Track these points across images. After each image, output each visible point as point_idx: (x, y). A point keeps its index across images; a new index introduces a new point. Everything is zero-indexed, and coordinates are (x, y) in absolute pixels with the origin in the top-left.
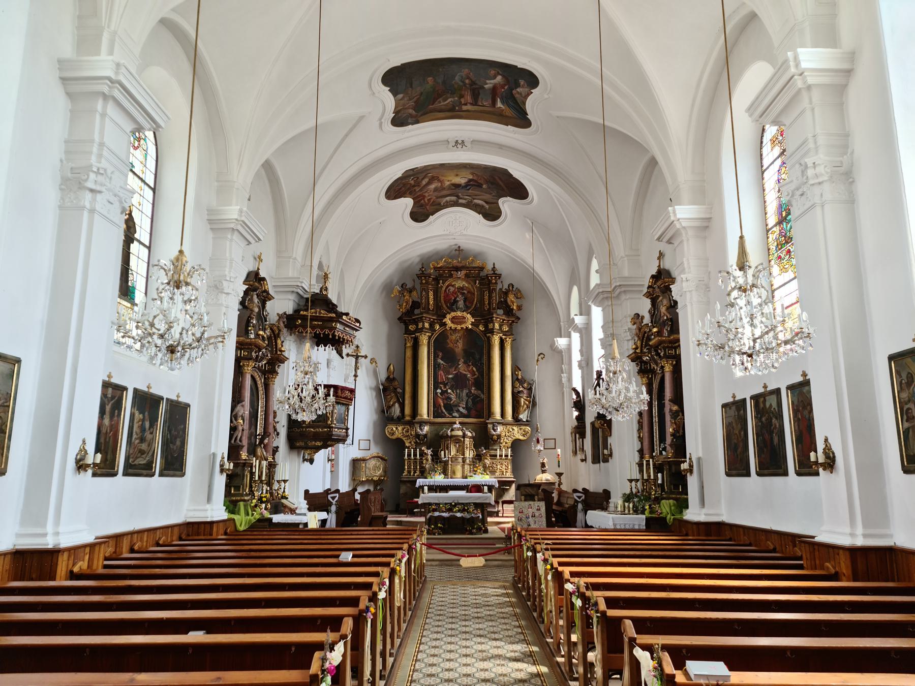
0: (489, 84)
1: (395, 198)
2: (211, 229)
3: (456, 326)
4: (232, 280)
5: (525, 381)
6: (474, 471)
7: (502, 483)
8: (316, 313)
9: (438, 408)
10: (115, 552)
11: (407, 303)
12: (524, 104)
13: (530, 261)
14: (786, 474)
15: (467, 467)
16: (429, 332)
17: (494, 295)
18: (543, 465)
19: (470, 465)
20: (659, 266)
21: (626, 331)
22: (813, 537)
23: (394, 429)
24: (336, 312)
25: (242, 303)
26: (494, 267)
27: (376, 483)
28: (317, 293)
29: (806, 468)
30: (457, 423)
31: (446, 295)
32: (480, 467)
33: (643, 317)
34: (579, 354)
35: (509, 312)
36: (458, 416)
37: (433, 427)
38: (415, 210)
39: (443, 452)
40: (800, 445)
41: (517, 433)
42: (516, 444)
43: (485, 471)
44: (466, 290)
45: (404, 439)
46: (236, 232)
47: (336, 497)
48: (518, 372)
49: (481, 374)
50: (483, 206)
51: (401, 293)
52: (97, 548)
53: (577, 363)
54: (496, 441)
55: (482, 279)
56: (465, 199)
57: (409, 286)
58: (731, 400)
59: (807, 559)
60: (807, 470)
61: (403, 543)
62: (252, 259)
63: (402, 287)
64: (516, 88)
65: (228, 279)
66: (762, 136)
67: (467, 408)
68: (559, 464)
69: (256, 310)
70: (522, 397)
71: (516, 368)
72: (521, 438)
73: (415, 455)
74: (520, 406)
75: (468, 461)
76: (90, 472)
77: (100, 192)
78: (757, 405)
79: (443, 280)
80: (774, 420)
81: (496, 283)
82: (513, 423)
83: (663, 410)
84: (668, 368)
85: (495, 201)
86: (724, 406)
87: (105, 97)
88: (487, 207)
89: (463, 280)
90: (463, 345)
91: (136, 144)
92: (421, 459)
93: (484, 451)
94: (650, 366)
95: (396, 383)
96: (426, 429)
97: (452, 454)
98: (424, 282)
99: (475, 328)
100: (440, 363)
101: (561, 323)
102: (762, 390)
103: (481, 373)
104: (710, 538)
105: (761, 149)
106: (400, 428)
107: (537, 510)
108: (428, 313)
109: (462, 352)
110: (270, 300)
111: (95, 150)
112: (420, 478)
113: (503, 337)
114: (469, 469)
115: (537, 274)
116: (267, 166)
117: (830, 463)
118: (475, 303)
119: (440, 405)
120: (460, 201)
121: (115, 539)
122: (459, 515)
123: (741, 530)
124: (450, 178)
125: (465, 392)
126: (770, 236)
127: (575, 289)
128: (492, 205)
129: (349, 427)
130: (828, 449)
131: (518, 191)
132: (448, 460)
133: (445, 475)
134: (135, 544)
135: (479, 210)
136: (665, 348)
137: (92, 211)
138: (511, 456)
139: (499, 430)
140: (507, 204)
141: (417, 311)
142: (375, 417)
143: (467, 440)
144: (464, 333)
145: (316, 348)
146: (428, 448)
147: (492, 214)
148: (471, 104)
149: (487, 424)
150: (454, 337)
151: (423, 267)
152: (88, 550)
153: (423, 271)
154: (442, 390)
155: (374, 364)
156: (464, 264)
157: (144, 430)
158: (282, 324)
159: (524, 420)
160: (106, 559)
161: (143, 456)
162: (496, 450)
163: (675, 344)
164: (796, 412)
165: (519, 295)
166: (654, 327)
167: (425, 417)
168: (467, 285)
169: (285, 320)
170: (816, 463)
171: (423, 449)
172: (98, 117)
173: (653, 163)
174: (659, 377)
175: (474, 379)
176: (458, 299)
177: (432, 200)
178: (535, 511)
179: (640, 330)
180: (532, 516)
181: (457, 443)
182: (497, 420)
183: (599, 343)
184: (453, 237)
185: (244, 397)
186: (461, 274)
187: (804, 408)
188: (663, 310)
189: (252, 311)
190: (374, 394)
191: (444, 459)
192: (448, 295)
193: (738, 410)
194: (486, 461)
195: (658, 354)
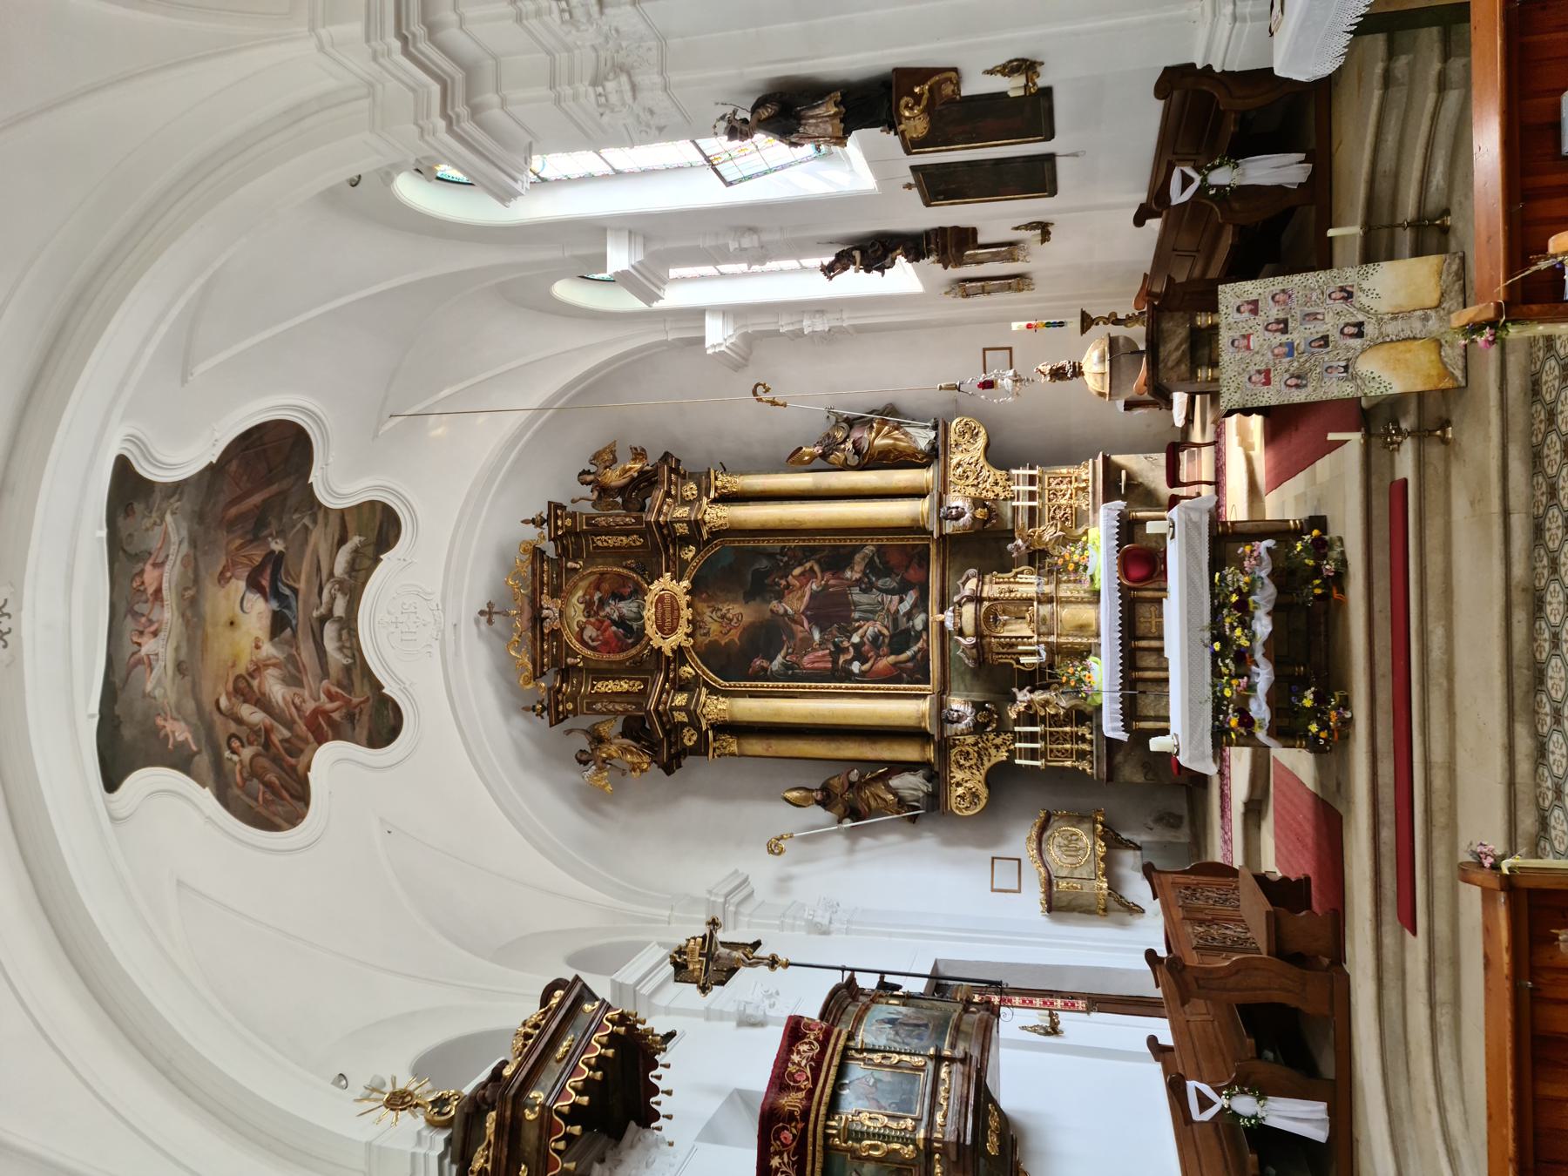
3: (683, 622)
5: (828, 435)
6: (1076, 571)
7: (1110, 493)
9: (903, 670)
11: (625, 750)
13: (512, 422)
15: (1065, 591)
17: (602, 521)
18: (1058, 374)
19: (1058, 582)
23: (960, 791)
26: (533, 521)
27: (1114, 841)
30: (940, 617)
31: (606, 646)
32: (1065, 552)
35: (644, 482)
36: (922, 616)
37: (954, 685)
38: (365, 733)
39: (1024, 660)
41: (968, 453)
42: (999, 457)
43: (1076, 541)
44: (592, 597)
45: (987, 765)
47: (1198, 1091)
48: (805, 454)
49: (809, 552)
50: (356, 551)
54: (990, 510)
55: (564, 553)
56: (333, 599)
57: (583, 743)
63: (585, 763)
67: (901, 591)
68: (1054, 325)
70: (871, 444)
71: (795, 462)
72: (981, 442)
73: (1032, 737)
74: (895, 447)
75: (1048, 589)
79: (567, 656)
81: (573, 516)
82: (941, 463)
85: (334, 522)
88: (355, 541)
89: (566, 602)
90: (734, 601)
93: (1019, 542)
96: (957, 704)
97: (1029, 633)
98: (570, 706)
99: (691, 571)
101: (670, 337)
106: (959, 775)
107: (1255, 311)
109: (752, 603)
112: (1099, 726)
113: (712, 495)
114: (1071, 586)
117: (1025, 67)
119: (895, 665)
120: (339, 609)
122: (1263, 626)
124: (246, 644)
125: (857, 596)
128: (351, 526)
132: (1047, 643)
133: (1089, 652)
135: (367, 563)
137: (795, 918)
138: (1031, 468)
139: (959, 503)
143: (990, 590)
144: (704, 601)
145: (661, 1122)
149: (943, 537)
150: (714, 627)
151: (534, 709)
153: (544, 709)
154: (853, 659)
155: (783, 844)
156: (526, 601)
159: (932, 434)
162: (1015, 509)
165: (605, 457)
167: (924, 706)
168: (580, 593)
171: (1013, 716)
175: (823, 571)
176: (615, 616)
177: (334, 689)
178: (1261, 319)
180: (1285, 331)
181: (996, 619)
182: (931, 509)
184: (450, 628)
186: (550, 607)
190: (866, 842)
191: (1044, 654)
192: (605, 643)
194: (1047, 537)
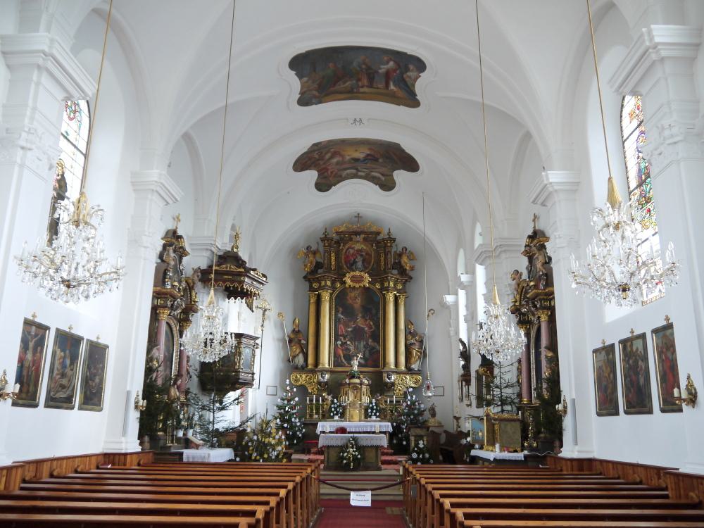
0: (383, 69)
1: (302, 169)
2: (134, 190)
3: (355, 284)
4: (151, 235)
8: (227, 268)
10: (35, 476)
11: (311, 263)
12: (414, 86)
13: (421, 226)
14: (650, 412)
17: (389, 256)
20: (534, 227)
21: (508, 284)
22: (678, 469)
24: (245, 268)
25: (161, 257)
28: (229, 251)
29: (671, 405)
33: (521, 274)
34: (465, 308)
35: (403, 272)
40: (664, 385)
45: (307, 386)
46: (156, 194)
50: (379, 178)
51: (306, 255)
52: (14, 471)
53: (463, 318)
55: (378, 242)
56: (364, 172)
57: (314, 248)
58: (602, 345)
59: (672, 489)
60: (671, 407)
61: (295, 476)
62: (172, 220)
63: (307, 249)
64: (406, 72)
65: (147, 233)
66: (622, 111)
69: (172, 263)
71: (408, 322)
76: (10, 401)
77: (30, 149)
78: (624, 349)
80: (640, 363)
81: (391, 246)
83: (540, 357)
84: (544, 318)
86: (595, 351)
87: (39, 67)
88: (383, 178)
90: (362, 301)
91: (72, 115)
94: (528, 317)
97: (350, 400)
98: (327, 244)
99: (372, 287)
102: (629, 335)
103: (377, 326)
104: (582, 473)
105: (621, 122)
106: (304, 376)
108: (329, 272)
110: (186, 255)
111: (28, 113)
115: (428, 238)
116: (187, 137)
117: (693, 399)
120: (360, 173)
121: (35, 465)
123: (611, 465)
124: (349, 153)
125: (363, 343)
126: (632, 197)
127: (461, 252)
129: (255, 371)
130: (691, 386)
131: (410, 164)
134: (54, 470)
136: (541, 300)
139: (393, 378)
140: (400, 176)
141: (320, 271)
142: (281, 365)
143: (364, 387)
146: (328, 395)
147: (387, 185)
148: (367, 86)
149: (382, 373)
152: (5, 472)
157: (66, 367)
158: (196, 278)
160: (24, 481)
161: (64, 390)
163: (550, 296)
164: (660, 353)
165: (412, 257)
166: (531, 281)
167: (327, 366)
169: (199, 274)
170: (680, 398)
172: (33, 86)
173: (528, 136)
174: (536, 327)
177: (334, 173)
179: (518, 285)
183: (483, 297)
185: (160, 342)
187: (668, 349)
188: (539, 265)
189: (168, 264)
190: (281, 344)
193: (608, 354)
195: (535, 306)
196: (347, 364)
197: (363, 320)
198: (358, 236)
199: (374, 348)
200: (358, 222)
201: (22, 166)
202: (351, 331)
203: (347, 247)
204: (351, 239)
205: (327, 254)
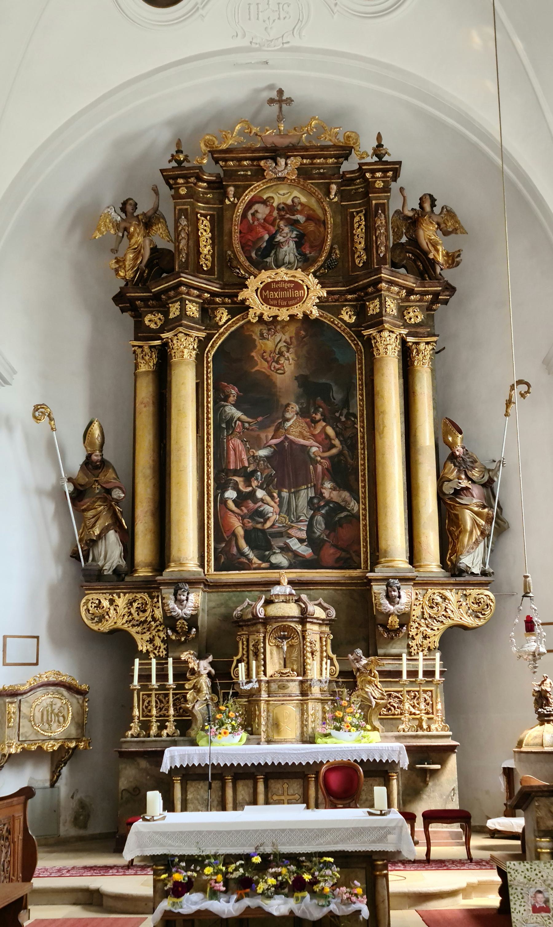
3: (274, 311)
5: (474, 461)
6: (335, 719)
9: (228, 543)
11: (138, 252)
15: (314, 708)
16: (199, 330)
17: (381, 221)
26: (380, 146)
30: (285, 581)
39: (242, 667)
43: (366, 719)
44: (300, 212)
45: (133, 631)
63: (123, 209)
72: (469, 621)
73: (162, 676)
74: (462, 531)
75: (316, 691)
79: (236, 187)
81: (386, 189)
82: (446, 580)
89: (293, 184)
90: (298, 366)
92: (180, 687)
93: (364, 661)
95: (111, 475)
97: (270, 672)
98: (183, 191)
99: (328, 319)
100: (232, 418)
109: (296, 383)
112: (175, 743)
114: (320, 714)
118: (327, 247)
119: (234, 534)
132: (259, 690)
138: (442, 673)
139: (404, 599)
144: (297, 333)
146: (200, 657)
149: (369, 582)
150: (270, 344)
151: (179, 152)
153: (179, 162)
162: (398, 657)
168: (303, 200)
175: (331, 458)
176: (279, 238)
181: (284, 638)
182: (398, 570)
184: (263, 56)
190: (50, 507)
191: (248, 687)
192: (251, 228)
194: (369, 689)
196: (255, 560)
197: (302, 423)
198: (282, 161)
199: (339, 508)
200: (280, 119)
201: (307, 488)
202: (267, 458)
203: (248, 199)
204: (259, 174)
205: (183, 222)
